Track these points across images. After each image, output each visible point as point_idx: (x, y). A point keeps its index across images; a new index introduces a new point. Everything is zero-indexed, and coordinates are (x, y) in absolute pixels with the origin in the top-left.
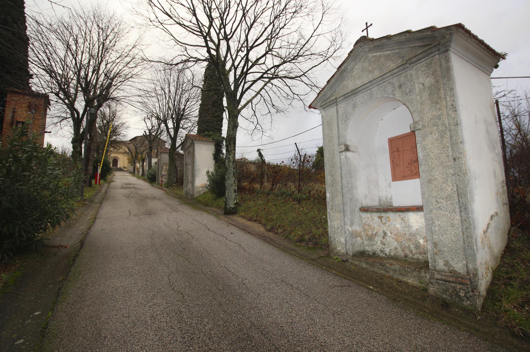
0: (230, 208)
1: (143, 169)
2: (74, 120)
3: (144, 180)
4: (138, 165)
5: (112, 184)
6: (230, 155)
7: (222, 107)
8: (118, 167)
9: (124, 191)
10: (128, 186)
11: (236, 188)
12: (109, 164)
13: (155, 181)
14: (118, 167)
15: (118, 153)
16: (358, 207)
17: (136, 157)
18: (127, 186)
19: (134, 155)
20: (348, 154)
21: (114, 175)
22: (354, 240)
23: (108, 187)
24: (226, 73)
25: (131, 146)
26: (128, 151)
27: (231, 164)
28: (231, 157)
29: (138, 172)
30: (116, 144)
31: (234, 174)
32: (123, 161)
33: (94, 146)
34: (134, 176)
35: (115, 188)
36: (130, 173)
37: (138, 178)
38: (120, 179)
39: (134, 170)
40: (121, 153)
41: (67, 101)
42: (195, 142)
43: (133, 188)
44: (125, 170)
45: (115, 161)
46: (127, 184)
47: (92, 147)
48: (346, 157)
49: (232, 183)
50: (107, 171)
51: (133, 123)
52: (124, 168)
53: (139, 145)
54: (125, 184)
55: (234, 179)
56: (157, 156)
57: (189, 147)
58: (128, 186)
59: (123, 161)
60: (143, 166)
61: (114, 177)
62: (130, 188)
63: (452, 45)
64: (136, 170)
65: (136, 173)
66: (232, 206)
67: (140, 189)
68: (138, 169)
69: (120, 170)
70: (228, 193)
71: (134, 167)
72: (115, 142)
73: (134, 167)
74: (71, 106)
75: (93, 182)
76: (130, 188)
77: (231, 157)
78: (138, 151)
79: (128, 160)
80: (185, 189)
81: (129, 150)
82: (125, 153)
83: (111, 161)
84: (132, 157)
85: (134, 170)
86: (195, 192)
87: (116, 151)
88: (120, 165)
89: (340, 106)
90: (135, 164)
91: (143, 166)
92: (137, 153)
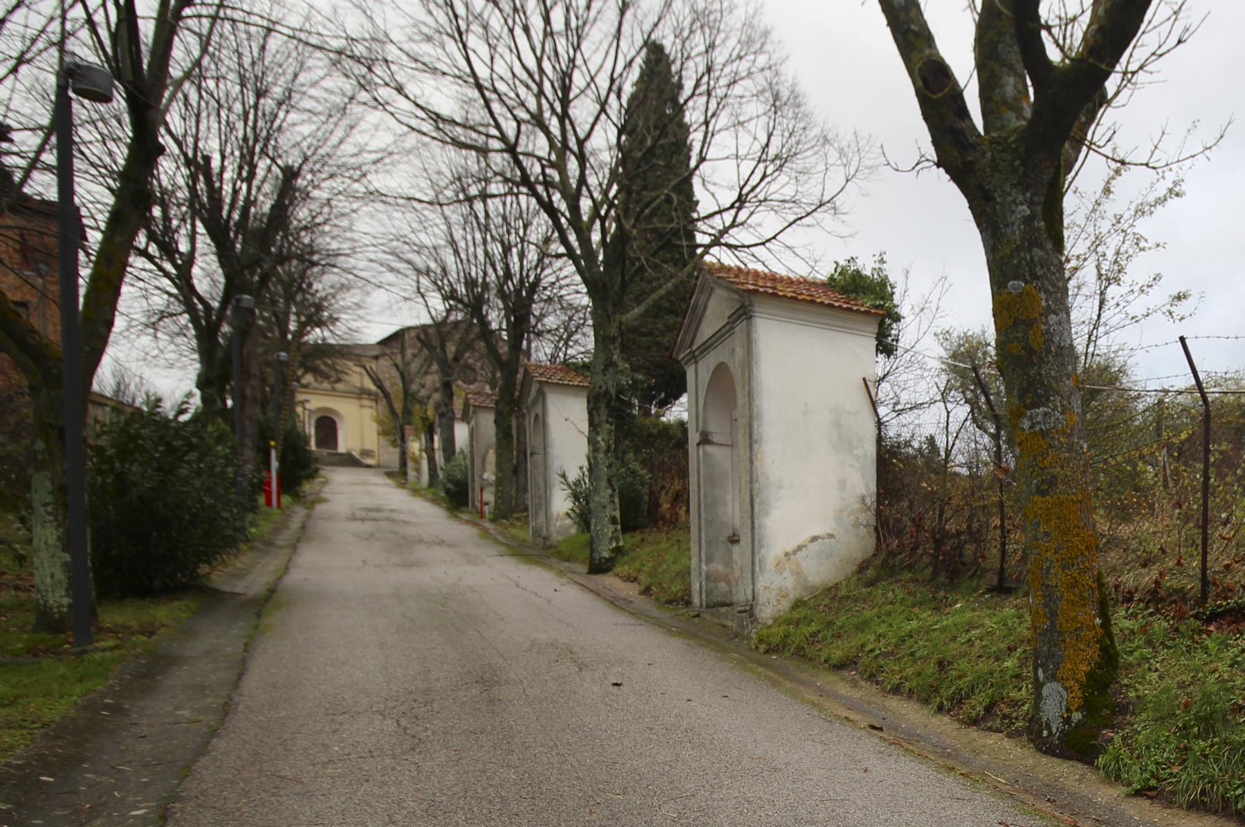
0: (600, 559)
1: (431, 460)
2: (195, 320)
3: (435, 501)
4: (415, 446)
5: (320, 508)
6: (598, 433)
7: (1031, 25)
8: (342, 448)
9: (356, 526)
10: (372, 514)
11: (617, 514)
12: (306, 440)
13: (466, 504)
14: (342, 448)
15: (333, 392)
16: (726, 535)
17: (407, 412)
18: (371, 514)
19: (398, 406)
20: (709, 448)
21: (326, 482)
22: (712, 585)
23: (308, 516)
24: (584, 226)
25: (385, 369)
26: (373, 388)
27: (601, 455)
28: (599, 438)
29: (418, 470)
30: (327, 361)
31: (609, 481)
32: (358, 427)
33: (253, 388)
34: (402, 486)
35: (330, 518)
36: (390, 475)
37: (416, 492)
38: (343, 491)
39: (404, 463)
40: (346, 395)
41: (168, 266)
42: (546, 389)
43: (387, 519)
44: (369, 461)
45: (327, 426)
46: (369, 510)
47: (248, 392)
48: (705, 453)
49: (605, 501)
50: (299, 469)
51: (377, 307)
52: (366, 453)
53: (414, 366)
54: (362, 509)
55: (610, 491)
56: (465, 418)
57: (535, 402)
58: (372, 514)
59: (358, 427)
60: (430, 450)
61: (326, 489)
62: (375, 520)
63: (756, 308)
64: (410, 464)
65: (411, 474)
66: (606, 554)
67: (406, 523)
68: (417, 461)
69: (350, 461)
70: (596, 525)
71: (403, 454)
72: (324, 350)
73: (403, 454)
74: (183, 280)
75: (262, 500)
76: (375, 520)
77: (599, 438)
78: (414, 387)
79: (380, 422)
80: (532, 524)
81: (378, 382)
82: (362, 393)
83: (311, 430)
84: (392, 410)
85: (404, 463)
86: (552, 529)
87: (326, 385)
88: (346, 442)
89: (700, 364)
90: (403, 439)
91: (430, 450)
92: (408, 396)
